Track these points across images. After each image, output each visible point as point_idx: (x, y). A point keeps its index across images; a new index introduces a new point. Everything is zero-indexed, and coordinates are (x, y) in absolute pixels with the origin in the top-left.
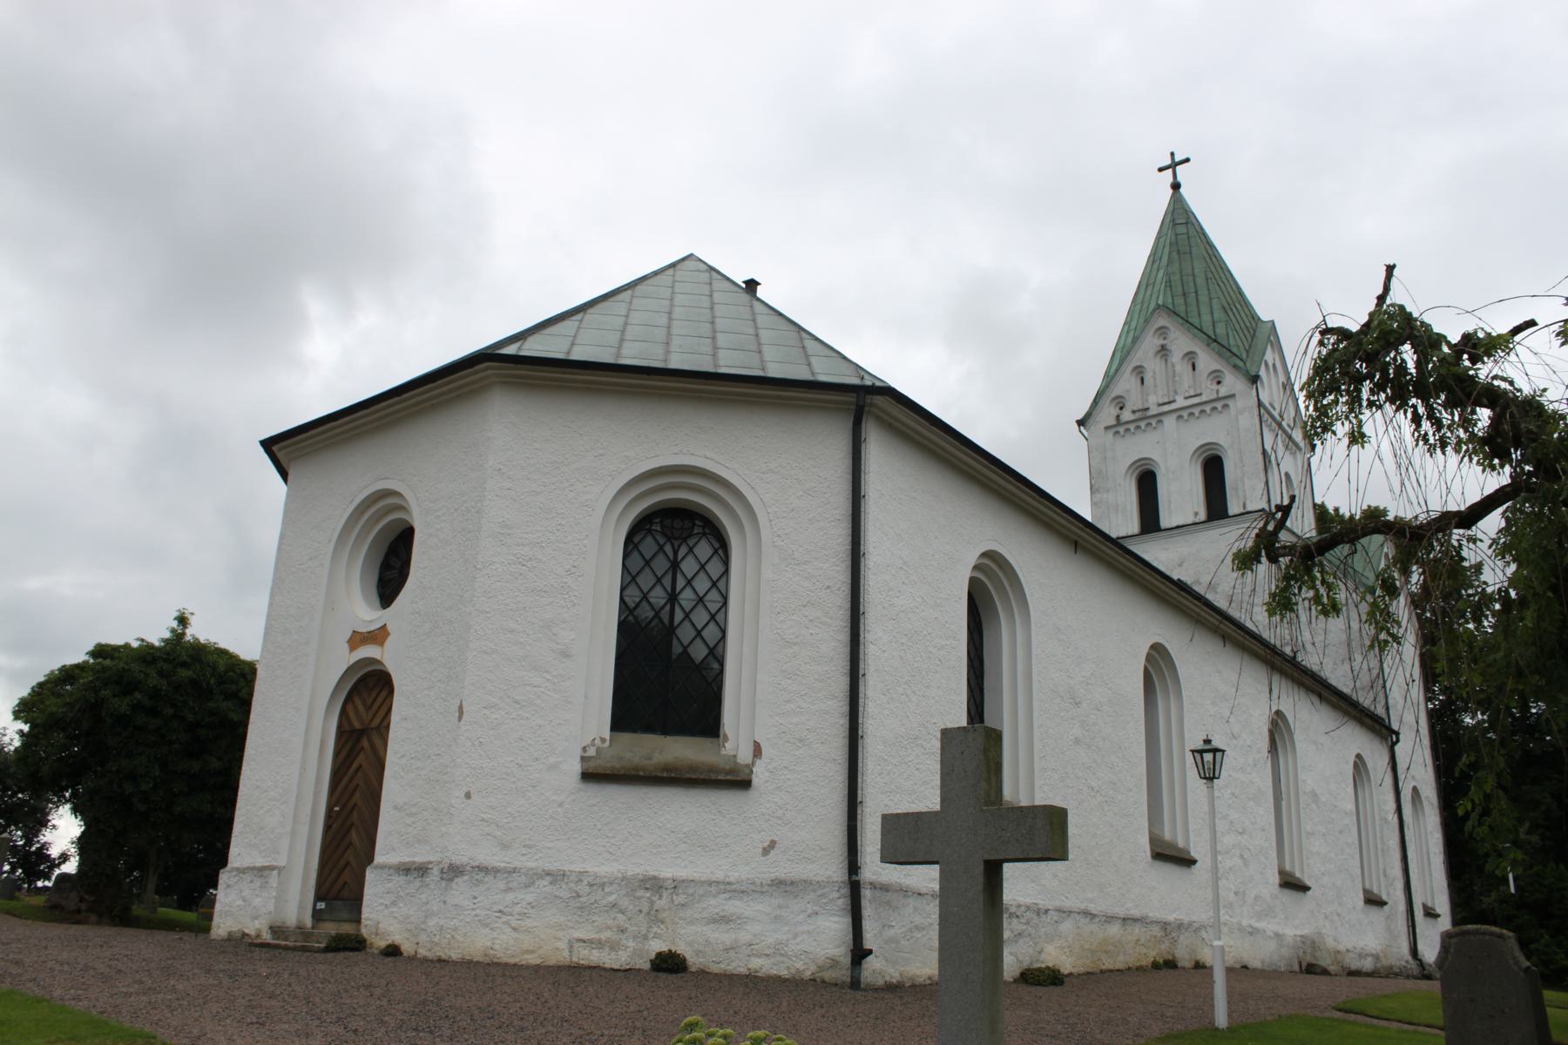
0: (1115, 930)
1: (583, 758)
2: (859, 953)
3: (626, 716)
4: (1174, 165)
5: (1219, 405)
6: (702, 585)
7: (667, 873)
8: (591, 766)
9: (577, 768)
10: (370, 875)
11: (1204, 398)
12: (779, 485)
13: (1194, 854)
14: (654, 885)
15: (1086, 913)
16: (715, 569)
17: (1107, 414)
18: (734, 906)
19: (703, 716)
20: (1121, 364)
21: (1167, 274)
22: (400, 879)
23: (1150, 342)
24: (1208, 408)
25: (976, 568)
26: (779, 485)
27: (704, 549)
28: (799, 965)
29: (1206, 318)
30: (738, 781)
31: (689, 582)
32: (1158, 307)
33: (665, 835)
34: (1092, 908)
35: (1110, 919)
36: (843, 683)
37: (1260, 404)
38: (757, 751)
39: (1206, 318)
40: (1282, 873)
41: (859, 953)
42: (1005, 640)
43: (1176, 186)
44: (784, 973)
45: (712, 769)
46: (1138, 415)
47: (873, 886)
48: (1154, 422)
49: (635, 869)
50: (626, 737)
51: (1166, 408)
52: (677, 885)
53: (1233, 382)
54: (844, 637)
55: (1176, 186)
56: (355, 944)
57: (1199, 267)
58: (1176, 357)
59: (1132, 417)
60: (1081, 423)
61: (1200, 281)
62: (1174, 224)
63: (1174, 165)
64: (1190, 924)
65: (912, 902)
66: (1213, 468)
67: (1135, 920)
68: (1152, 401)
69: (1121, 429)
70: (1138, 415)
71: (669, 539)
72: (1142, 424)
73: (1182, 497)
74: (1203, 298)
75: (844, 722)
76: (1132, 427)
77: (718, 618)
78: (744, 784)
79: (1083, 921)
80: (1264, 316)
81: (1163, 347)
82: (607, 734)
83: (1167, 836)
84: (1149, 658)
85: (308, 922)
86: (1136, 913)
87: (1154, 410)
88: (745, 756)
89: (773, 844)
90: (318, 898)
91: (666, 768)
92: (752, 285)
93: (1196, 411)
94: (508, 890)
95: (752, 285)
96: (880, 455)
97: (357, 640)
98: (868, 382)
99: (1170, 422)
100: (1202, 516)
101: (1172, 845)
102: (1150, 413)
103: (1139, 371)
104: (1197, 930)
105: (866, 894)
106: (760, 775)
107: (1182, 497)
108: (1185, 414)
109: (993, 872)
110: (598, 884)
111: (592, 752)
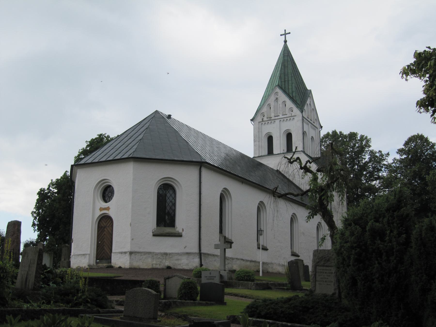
0: (248, 263)
1: (153, 232)
2: (201, 265)
3: (158, 224)
4: (285, 34)
5: (292, 118)
6: (171, 198)
7: (168, 251)
8: (154, 233)
9: (152, 234)
10: (112, 254)
11: (287, 116)
12: (185, 180)
13: (268, 248)
14: (166, 254)
15: (242, 259)
16: (173, 196)
17: (259, 119)
18: (179, 257)
19: (172, 224)
20: (264, 103)
21: (280, 74)
22: (120, 255)
23: (273, 98)
24: (288, 119)
25: (222, 191)
26: (185, 180)
27: (171, 192)
28: (191, 267)
29: (290, 91)
30: (180, 235)
31: (168, 198)
32: (276, 86)
33: (167, 245)
34: (244, 258)
35: (247, 261)
36: (198, 218)
37: (303, 117)
38: (183, 230)
39: (290, 91)
40: (292, 252)
41: (201, 265)
42: (227, 204)
43: (285, 42)
44: (188, 269)
45: (175, 233)
46: (268, 119)
47: (203, 254)
48: (273, 121)
49: (163, 251)
50: (159, 228)
51: (277, 118)
52: (170, 254)
53: (296, 111)
54: (198, 209)
55: (285, 42)
56: (112, 267)
57: (290, 71)
58: (280, 102)
59: (267, 120)
60: (252, 120)
61: (290, 76)
62: (284, 56)
63: (285, 34)
64: (266, 263)
65: (210, 256)
66: (289, 136)
67: (253, 261)
68: (272, 115)
69: (263, 123)
70: (268, 119)
71: (165, 190)
72: (270, 122)
73: (279, 145)
74: (290, 82)
75: (198, 224)
76: (267, 122)
77: (174, 204)
78: (181, 236)
79: (242, 261)
80: (308, 88)
81: (277, 99)
82: (156, 227)
83: (295, 251)
84: (259, 204)
85: (95, 264)
86: (253, 260)
87: (273, 118)
88: (180, 231)
89: (186, 246)
90: (97, 259)
91: (167, 233)
92: (169, 117)
93: (285, 119)
94: (141, 256)
95: (169, 117)
96: (205, 172)
97: (101, 209)
98: (203, 160)
99: (277, 122)
100: (286, 151)
101: (295, 253)
102: (272, 119)
103: (269, 105)
104: (268, 264)
105: (202, 255)
106: (183, 234)
107: (279, 145)
108: (282, 120)
109: (225, 249)
110: (157, 254)
111: (154, 231)
